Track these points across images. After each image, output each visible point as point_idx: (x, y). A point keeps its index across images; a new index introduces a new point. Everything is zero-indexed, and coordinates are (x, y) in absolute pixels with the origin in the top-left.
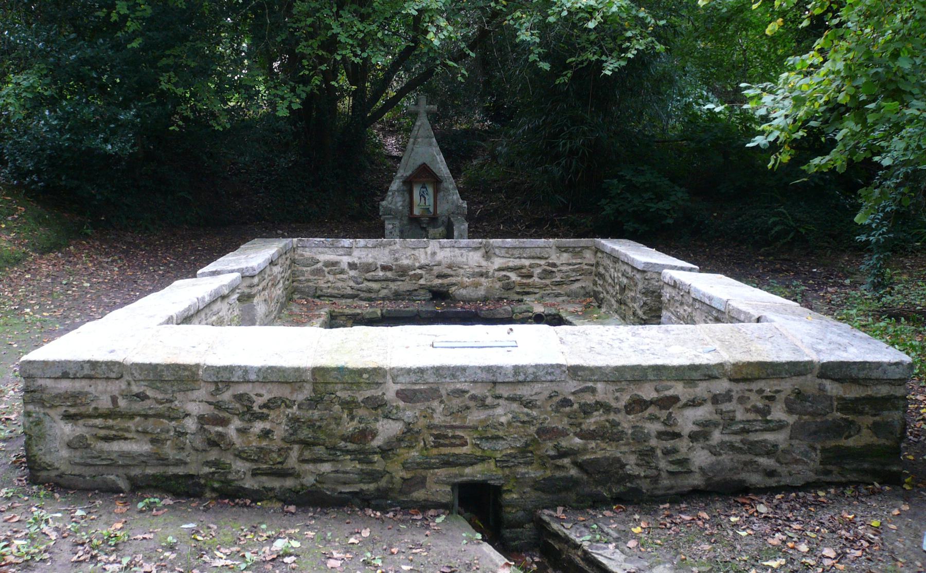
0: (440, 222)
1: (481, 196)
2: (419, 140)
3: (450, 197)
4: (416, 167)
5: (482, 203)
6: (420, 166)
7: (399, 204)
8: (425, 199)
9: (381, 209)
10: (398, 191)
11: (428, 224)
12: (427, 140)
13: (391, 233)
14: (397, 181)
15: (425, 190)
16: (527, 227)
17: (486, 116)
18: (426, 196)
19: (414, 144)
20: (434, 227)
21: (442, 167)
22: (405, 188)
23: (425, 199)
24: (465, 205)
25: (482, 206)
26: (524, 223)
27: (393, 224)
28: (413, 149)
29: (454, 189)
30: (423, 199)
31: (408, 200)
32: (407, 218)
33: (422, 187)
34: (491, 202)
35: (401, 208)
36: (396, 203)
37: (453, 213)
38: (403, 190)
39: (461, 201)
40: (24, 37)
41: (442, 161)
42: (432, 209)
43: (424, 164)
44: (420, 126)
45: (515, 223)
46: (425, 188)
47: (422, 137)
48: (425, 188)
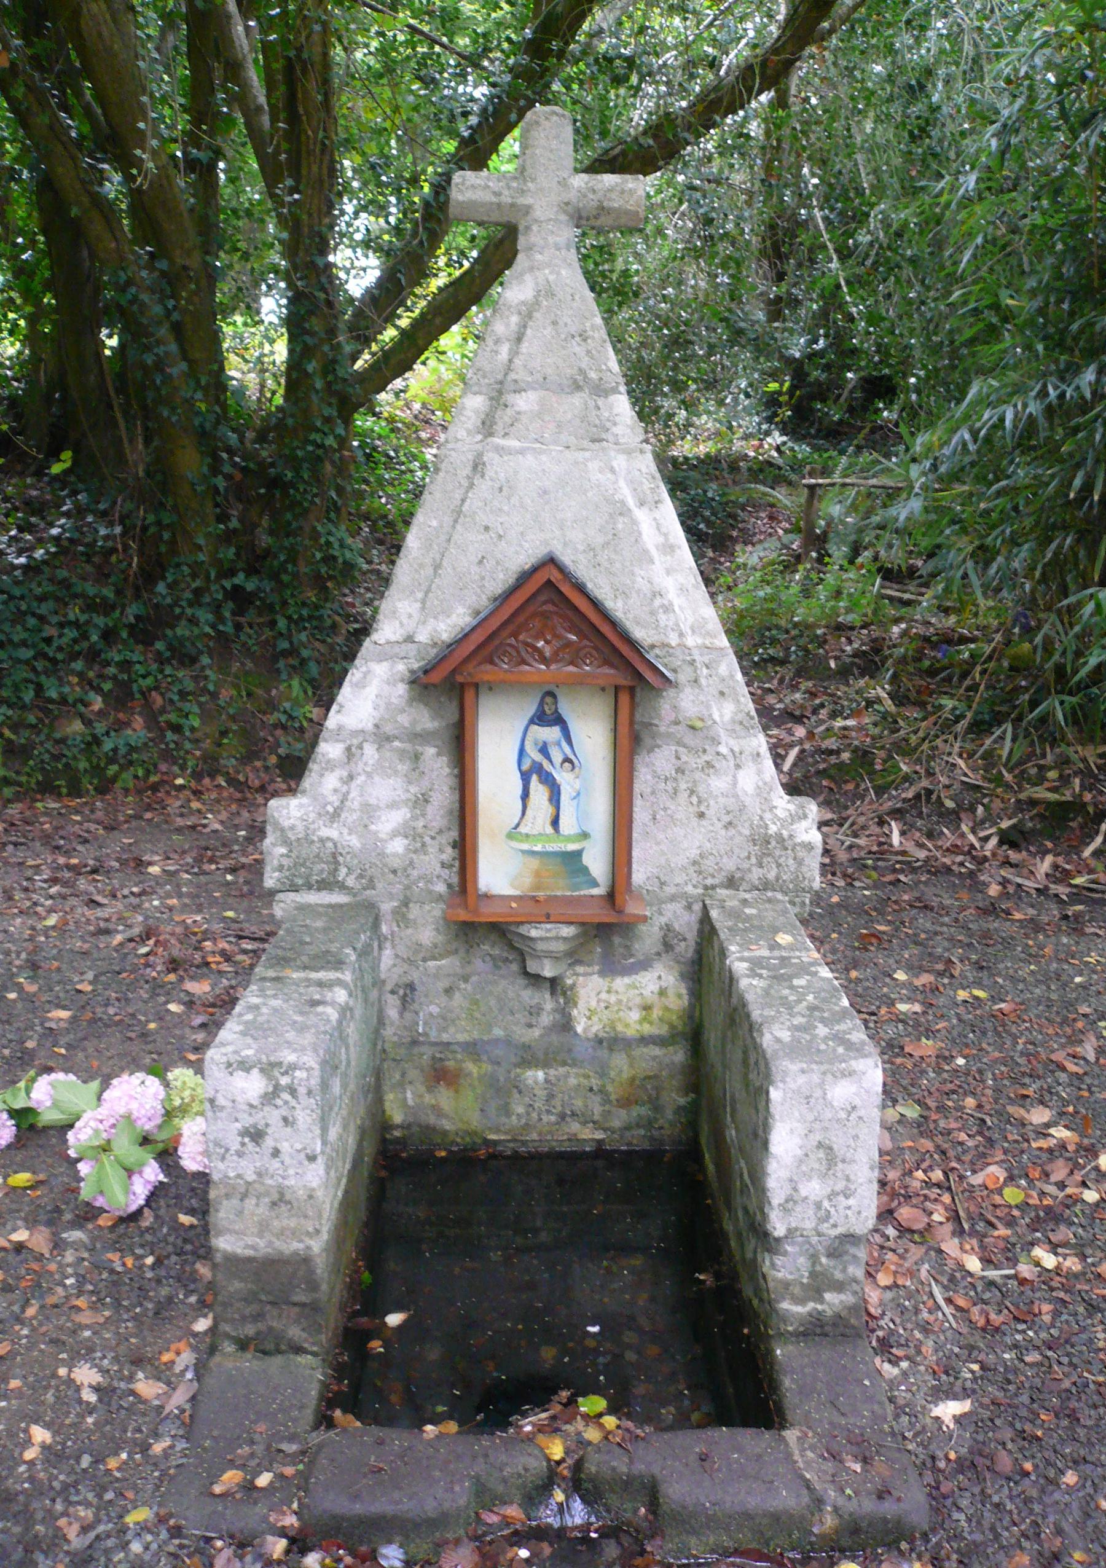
0: (649, 938)
1: (795, 688)
2: (524, 402)
3: (718, 784)
4: (499, 581)
5: (799, 720)
6: (525, 577)
7: (390, 821)
9: (274, 849)
10: (382, 738)
11: (574, 956)
12: (577, 400)
13: (256, 1135)
14: (381, 670)
15: (552, 733)
16: (1008, 840)
17: (769, 420)
18: (563, 777)
19: (487, 427)
20: (611, 968)
21: (670, 585)
22: (426, 720)
24: (809, 833)
25: (800, 732)
26: (991, 818)
27: (269, 1069)
28: (478, 466)
29: (740, 726)
30: (539, 792)
31: (443, 796)
32: (437, 910)
33: (541, 718)
34: (834, 715)
35: (398, 846)
36: (369, 811)
37: (731, 883)
38: (419, 737)
39: (783, 803)
40: (205, 399)
41: (669, 548)
42: (597, 861)
43: (551, 561)
44: (528, 313)
45: (953, 818)
46: (558, 720)
47: (544, 383)
48: (558, 720)
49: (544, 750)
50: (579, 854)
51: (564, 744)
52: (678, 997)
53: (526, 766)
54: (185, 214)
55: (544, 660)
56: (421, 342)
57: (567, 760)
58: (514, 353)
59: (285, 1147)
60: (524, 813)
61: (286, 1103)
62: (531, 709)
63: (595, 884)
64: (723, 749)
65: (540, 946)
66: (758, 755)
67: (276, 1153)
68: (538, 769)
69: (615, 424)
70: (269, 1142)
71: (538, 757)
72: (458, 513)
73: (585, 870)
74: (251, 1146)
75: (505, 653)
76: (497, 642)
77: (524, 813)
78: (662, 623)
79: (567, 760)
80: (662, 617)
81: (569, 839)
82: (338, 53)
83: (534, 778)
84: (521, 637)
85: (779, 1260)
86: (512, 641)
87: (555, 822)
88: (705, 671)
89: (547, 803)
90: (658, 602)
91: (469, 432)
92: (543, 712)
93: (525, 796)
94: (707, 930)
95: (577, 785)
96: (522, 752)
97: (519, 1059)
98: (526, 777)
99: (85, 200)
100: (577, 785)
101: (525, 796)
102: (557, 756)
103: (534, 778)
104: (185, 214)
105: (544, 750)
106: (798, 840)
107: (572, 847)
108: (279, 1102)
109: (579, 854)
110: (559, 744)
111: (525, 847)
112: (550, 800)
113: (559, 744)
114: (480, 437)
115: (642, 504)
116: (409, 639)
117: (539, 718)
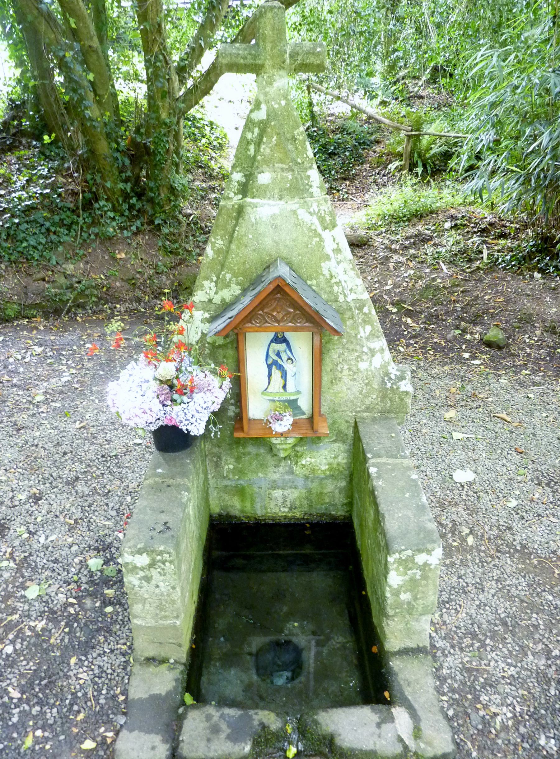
8: (284, 375)
15: (282, 347)
18: (288, 366)
23: (284, 375)
30: (276, 374)
33: (277, 340)
46: (284, 340)
48: (284, 340)
49: (278, 354)
50: (296, 401)
51: (288, 351)
52: (342, 459)
53: (270, 362)
54: (87, 17)
55: (278, 322)
56: (213, 79)
57: (289, 359)
58: (257, 150)
59: (161, 584)
60: (269, 383)
61: (160, 567)
62: (271, 335)
63: (304, 413)
64: (365, 349)
65: (278, 446)
66: (383, 349)
67: (157, 586)
68: (275, 363)
69: (311, 186)
70: (154, 582)
71: (276, 358)
72: (232, 236)
73: (299, 408)
74: (145, 584)
75: (257, 318)
76: (254, 313)
77: (269, 383)
78: (335, 291)
79: (289, 359)
80: (336, 288)
81: (291, 394)
82: (108, 234)
83: (274, 367)
84: (265, 311)
85: (390, 622)
86: (261, 312)
87: (284, 387)
88: (357, 312)
89: (280, 378)
90: (334, 280)
91: (236, 194)
92: (277, 337)
93: (270, 375)
94: (356, 423)
95: (295, 370)
96: (267, 355)
97: (270, 486)
98: (270, 367)
99: (35, 12)
100: (295, 370)
101: (270, 375)
102: (284, 357)
103: (274, 367)
104: (87, 17)
105: (278, 354)
106: (401, 390)
107: (292, 398)
108: (157, 567)
109: (296, 401)
110: (285, 351)
111: (271, 398)
112: (282, 377)
113: (285, 351)
114: (240, 196)
115: (325, 228)
116: (210, 301)
117: (276, 340)
